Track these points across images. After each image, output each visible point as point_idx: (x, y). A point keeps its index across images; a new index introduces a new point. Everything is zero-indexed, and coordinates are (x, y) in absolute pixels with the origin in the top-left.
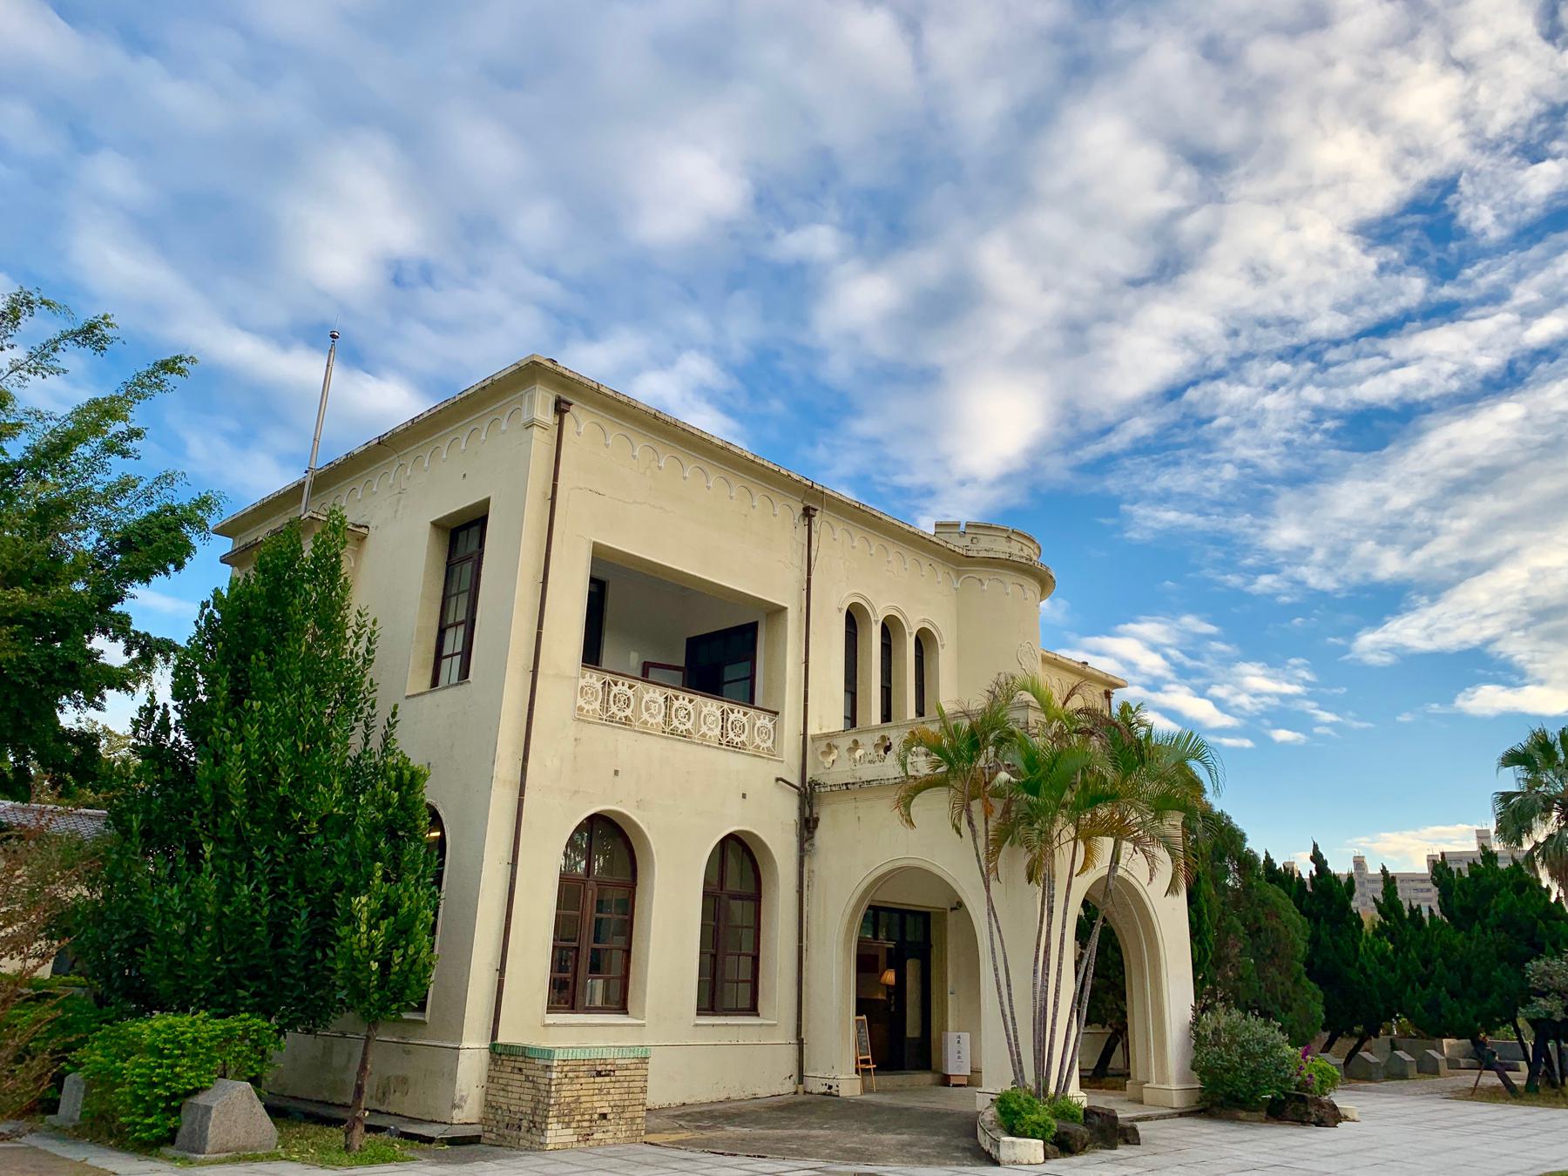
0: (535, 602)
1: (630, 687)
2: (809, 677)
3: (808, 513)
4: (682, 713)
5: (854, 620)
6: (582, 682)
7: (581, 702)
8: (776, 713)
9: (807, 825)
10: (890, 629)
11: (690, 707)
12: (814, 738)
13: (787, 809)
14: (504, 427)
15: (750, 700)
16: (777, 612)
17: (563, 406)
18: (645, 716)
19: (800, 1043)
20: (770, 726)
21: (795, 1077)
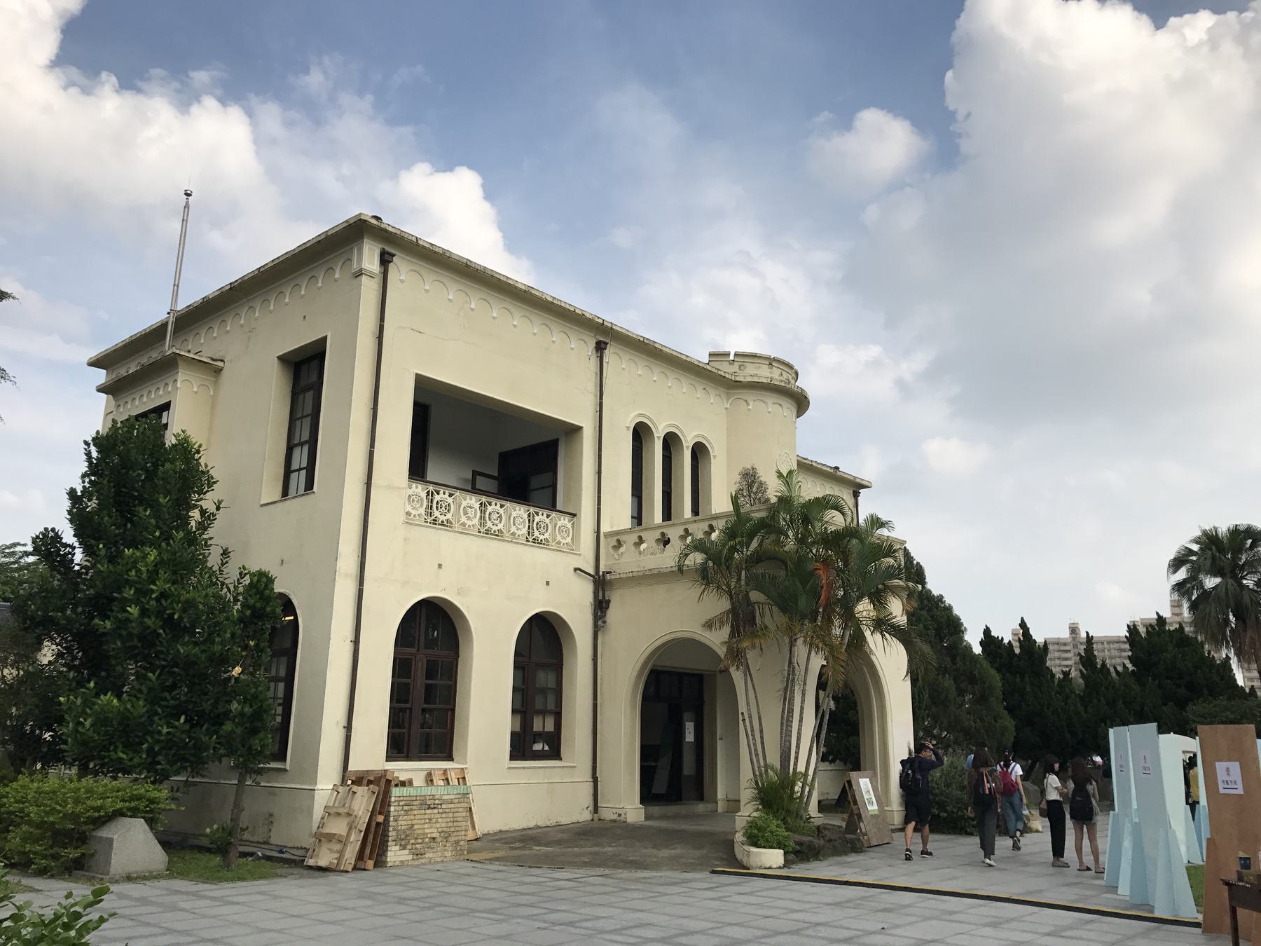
0: (370, 428)
1: (450, 495)
2: (602, 484)
3: (600, 347)
4: (495, 516)
5: (640, 434)
6: (410, 492)
7: (409, 509)
8: (574, 515)
9: (601, 607)
10: (671, 442)
11: (501, 511)
12: (608, 535)
13: (584, 592)
14: (337, 276)
15: (552, 506)
16: (577, 430)
17: (387, 257)
18: (463, 519)
19: (595, 780)
20: (569, 525)
21: (591, 808)
